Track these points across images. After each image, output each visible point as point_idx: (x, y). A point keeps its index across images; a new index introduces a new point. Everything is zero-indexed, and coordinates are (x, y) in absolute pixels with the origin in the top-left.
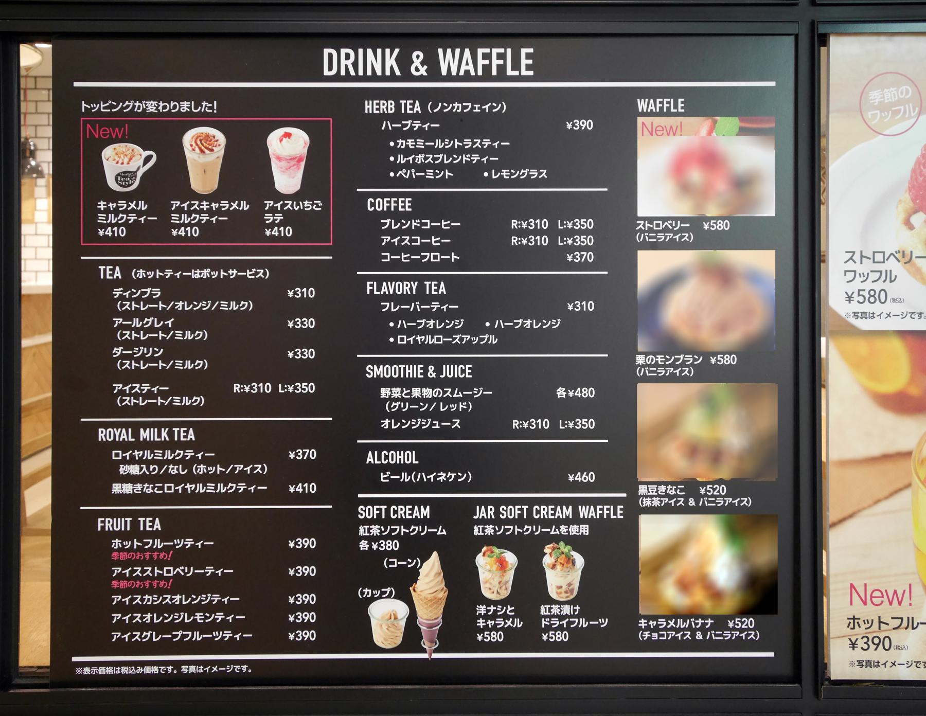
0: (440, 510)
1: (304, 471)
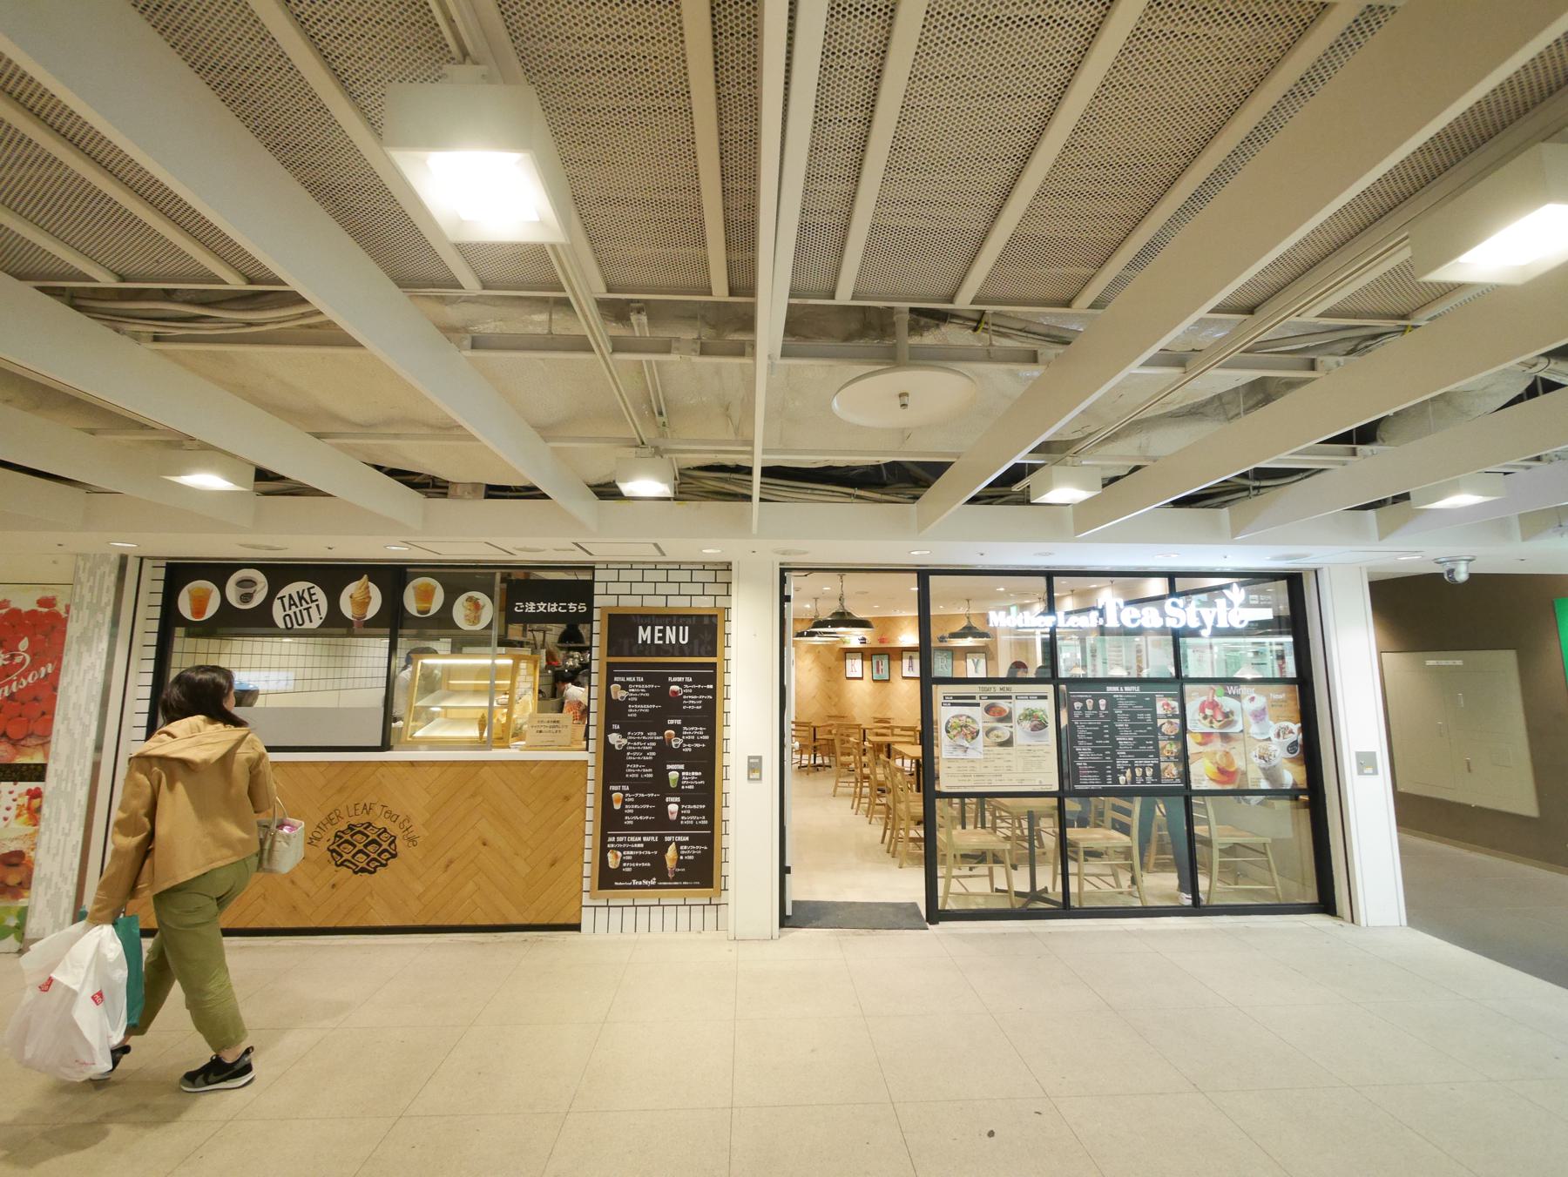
0: (1130, 762)
1: (1108, 755)
